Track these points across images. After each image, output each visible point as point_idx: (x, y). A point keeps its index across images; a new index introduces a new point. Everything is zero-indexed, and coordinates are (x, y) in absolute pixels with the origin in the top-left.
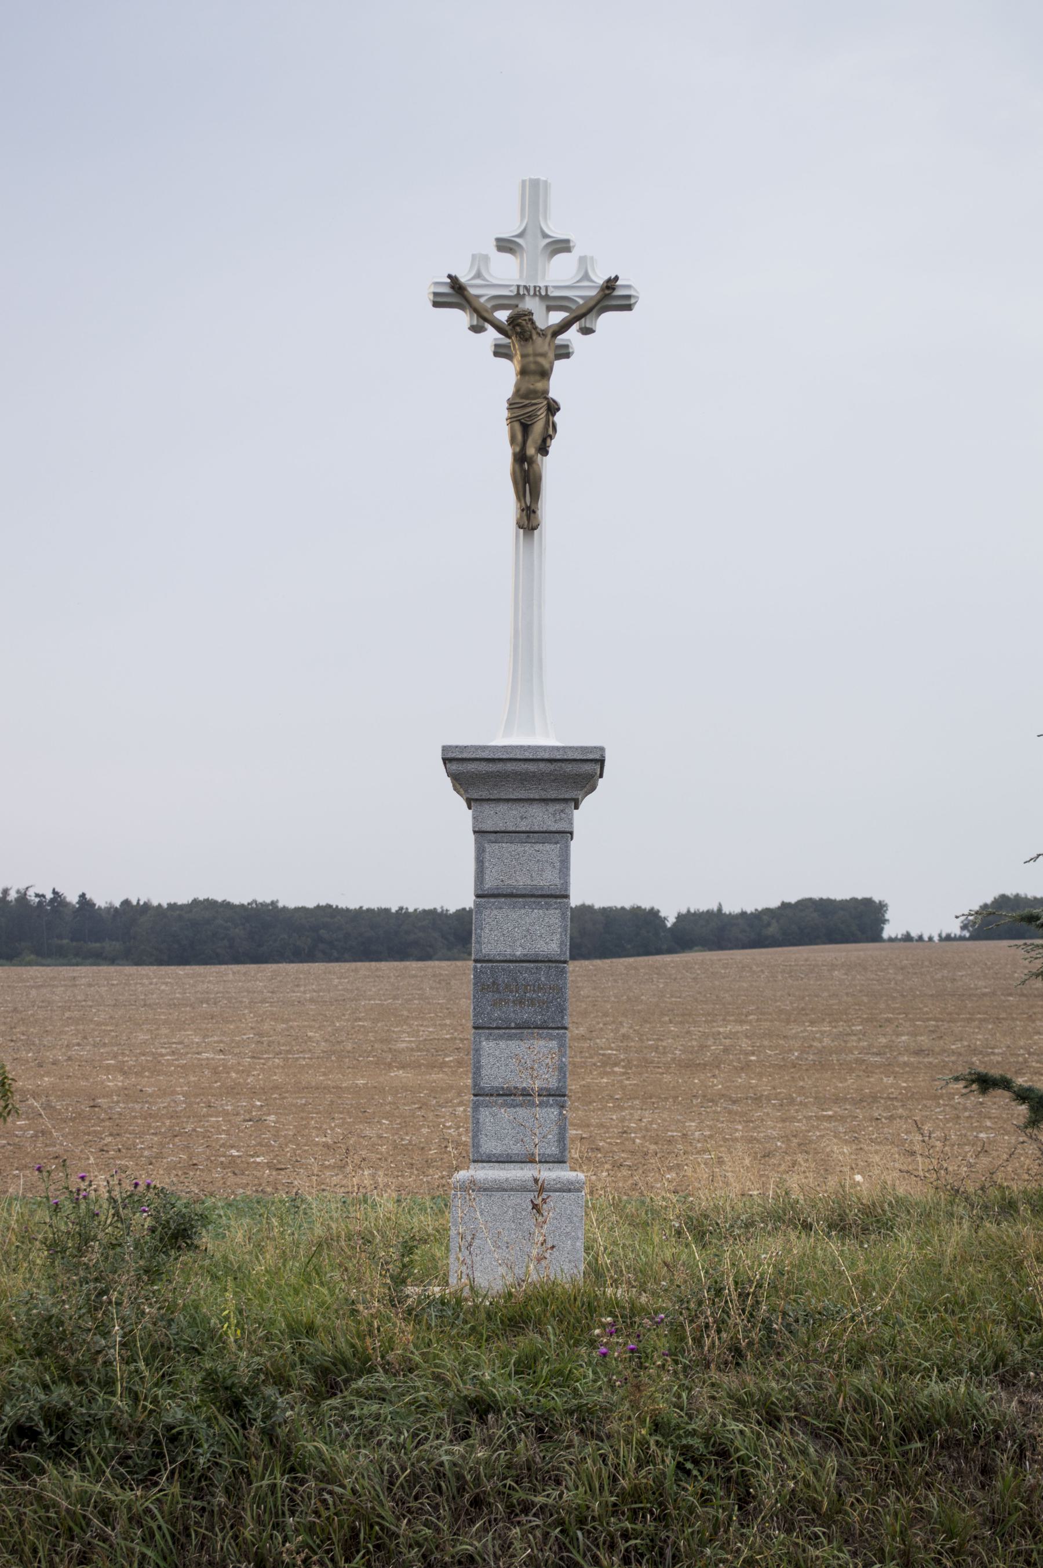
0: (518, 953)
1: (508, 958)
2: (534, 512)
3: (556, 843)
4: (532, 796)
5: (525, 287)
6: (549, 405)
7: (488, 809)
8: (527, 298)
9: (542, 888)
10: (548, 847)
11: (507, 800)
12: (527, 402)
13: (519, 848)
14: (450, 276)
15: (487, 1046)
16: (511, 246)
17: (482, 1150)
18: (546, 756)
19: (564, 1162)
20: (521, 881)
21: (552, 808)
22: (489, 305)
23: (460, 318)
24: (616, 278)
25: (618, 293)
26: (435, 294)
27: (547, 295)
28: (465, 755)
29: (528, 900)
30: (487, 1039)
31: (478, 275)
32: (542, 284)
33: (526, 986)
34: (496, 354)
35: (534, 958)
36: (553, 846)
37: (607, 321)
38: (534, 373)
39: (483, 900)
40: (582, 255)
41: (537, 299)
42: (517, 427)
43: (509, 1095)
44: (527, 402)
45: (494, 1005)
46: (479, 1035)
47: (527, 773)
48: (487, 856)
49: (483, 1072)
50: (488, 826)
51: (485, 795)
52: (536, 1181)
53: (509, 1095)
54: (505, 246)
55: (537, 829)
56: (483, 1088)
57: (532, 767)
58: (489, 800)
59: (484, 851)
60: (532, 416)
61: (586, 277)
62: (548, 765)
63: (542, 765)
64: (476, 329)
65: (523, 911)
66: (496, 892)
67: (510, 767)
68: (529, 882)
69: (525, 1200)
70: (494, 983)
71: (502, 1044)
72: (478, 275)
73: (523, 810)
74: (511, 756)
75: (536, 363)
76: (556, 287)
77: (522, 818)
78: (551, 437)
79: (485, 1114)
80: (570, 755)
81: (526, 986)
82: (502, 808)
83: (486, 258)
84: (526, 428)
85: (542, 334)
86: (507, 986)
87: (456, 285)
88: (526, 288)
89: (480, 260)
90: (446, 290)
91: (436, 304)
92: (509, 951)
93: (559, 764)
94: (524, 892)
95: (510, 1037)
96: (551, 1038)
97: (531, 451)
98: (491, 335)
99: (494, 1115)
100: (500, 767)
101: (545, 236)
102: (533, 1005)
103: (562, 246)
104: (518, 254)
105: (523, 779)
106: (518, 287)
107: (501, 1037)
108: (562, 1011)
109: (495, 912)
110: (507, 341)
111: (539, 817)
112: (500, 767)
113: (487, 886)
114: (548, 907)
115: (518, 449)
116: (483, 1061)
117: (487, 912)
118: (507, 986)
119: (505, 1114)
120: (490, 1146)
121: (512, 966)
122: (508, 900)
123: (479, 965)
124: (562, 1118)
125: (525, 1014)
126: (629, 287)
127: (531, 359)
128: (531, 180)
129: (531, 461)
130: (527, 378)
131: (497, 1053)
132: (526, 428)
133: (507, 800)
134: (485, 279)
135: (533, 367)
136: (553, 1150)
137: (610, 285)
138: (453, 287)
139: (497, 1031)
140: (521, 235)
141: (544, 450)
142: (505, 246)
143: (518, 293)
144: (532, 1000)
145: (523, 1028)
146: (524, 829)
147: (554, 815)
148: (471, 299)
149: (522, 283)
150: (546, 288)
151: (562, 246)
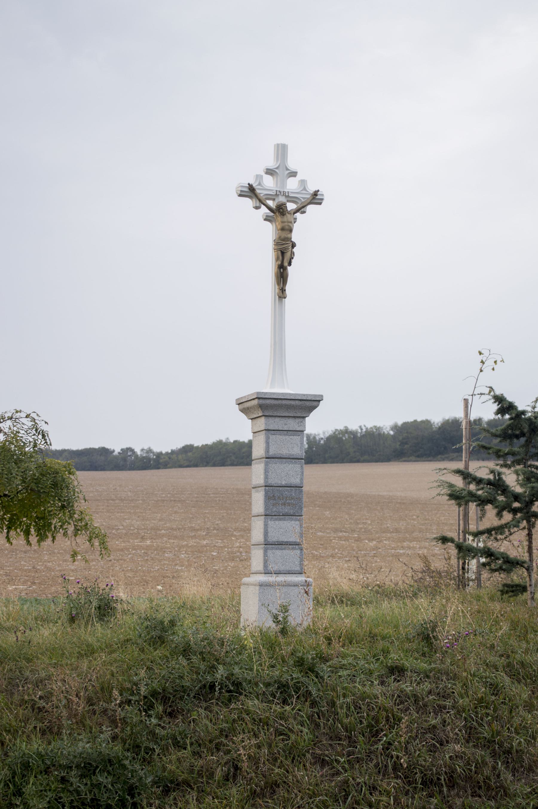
0: (283, 483)
1: (279, 485)
2: (285, 290)
3: (299, 436)
4: (290, 415)
5: (279, 191)
6: (292, 244)
7: (271, 420)
8: (280, 196)
9: (293, 455)
10: (295, 437)
11: (279, 416)
12: (284, 242)
13: (284, 437)
14: (249, 184)
15: (271, 523)
16: (272, 172)
17: (269, 569)
18: (300, 398)
19: (302, 573)
20: (285, 452)
21: (297, 420)
22: (264, 197)
23: (249, 202)
24: (318, 191)
25: (318, 197)
26: (241, 191)
27: (288, 196)
28: (266, 397)
29: (287, 460)
30: (271, 520)
31: (260, 184)
32: (286, 191)
33: (286, 498)
34: (296, 173)
35: (289, 485)
36: (297, 437)
37: (310, 208)
38: (287, 230)
39: (269, 460)
40: (303, 179)
41: (284, 197)
42: (280, 253)
43: (280, 544)
44: (284, 242)
45: (273, 505)
46: (267, 518)
47: (290, 405)
48: (270, 440)
49: (269, 535)
50: (271, 427)
51: (271, 414)
52: (306, 581)
53: (280, 544)
54: (270, 172)
55: (291, 429)
56: (269, 542)
57: (293, 403)
58: (272, 416)
59: (269, 438)
60: (286, 249)
61: (305, 189)
62: (300, 402)
63: (297, 402)
64: (257, 208)
65: (285, 465)
66: (274, 456)
67: (284, 402)
68: (288, 452)
69: (301, 590)
70: (273, 496)
71: (277, 522)
72: (260, 184)
73: (286, 421)
74: (285, 398)
75: (288, 225)
76: (291, 192)
77: (285, 424)
78: (293, 258)
79: (270, 552)
80: (309, 398)
81: (286, 498)
82: (277, 419)
83: (261, 177)
84: (283, 253)
85: (289, 213)
86: (279, 497)
87: (251, 189)
88: (280, 192)
89: (259, 177)
90: (247, 190)
91: (240, 195)
92: (279, 482)
93: (304, 402)
94: (286, 457)
95: (280, 520)
96: (296, 520)
97: (286, 264)
98: (264, 210)
99: (273, 553)
100: (280, 402)
101: (287, 169)
102: (289, 506)
103: (293, 174)
104: (275, 177)
105: (288, 408)
106: (277, 191)
107: (276, 520)
108: (301, 508)
109: (274, 465)
110: (272, 214)
111: (292, 424)
112: (280, 402)
113: (270, 454)
114: (296, 463)
115: (280, 263)
116: (269, 530)
117: (271, 465)
118: (279, 497)
119: (278, 553)
120: (272, 567)
121: (281, 488)
122: (279, 460)
123: (267, 488)
124: (301, 554)
125: (287, 510)
126: (323, 195)
127: (286, 224)
128: (282, 144)
129: (285, 269)
130: (284, 232)
131: (275, 526)
132: (283, 253)
133: (279, 416)
134: (262, 186)
135: (287, 227)
136: (298, 568)
137: (316, 194)
138: (250, 189)
139: (274, 517)
140: (277, 168)
141: (290, 264)
142: (270, 172)
143: (276, 194)
144: (289, 503)
145: (286, 515)
146: (286, 429)
147: (298, 423)
148: (258, 195)
149: (278, 190)
150: (288, 192)
151: (293, 174)
